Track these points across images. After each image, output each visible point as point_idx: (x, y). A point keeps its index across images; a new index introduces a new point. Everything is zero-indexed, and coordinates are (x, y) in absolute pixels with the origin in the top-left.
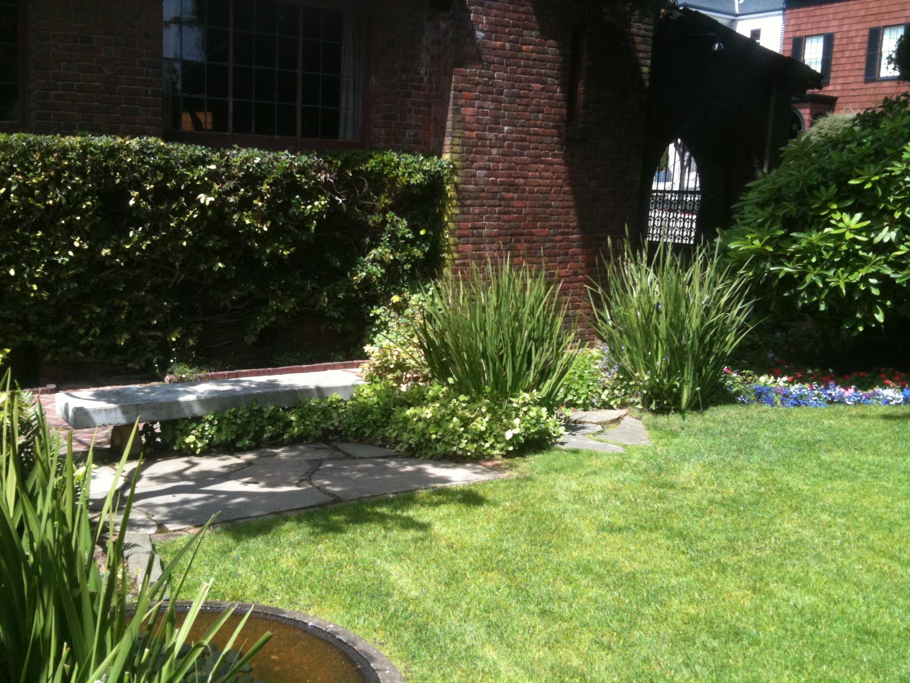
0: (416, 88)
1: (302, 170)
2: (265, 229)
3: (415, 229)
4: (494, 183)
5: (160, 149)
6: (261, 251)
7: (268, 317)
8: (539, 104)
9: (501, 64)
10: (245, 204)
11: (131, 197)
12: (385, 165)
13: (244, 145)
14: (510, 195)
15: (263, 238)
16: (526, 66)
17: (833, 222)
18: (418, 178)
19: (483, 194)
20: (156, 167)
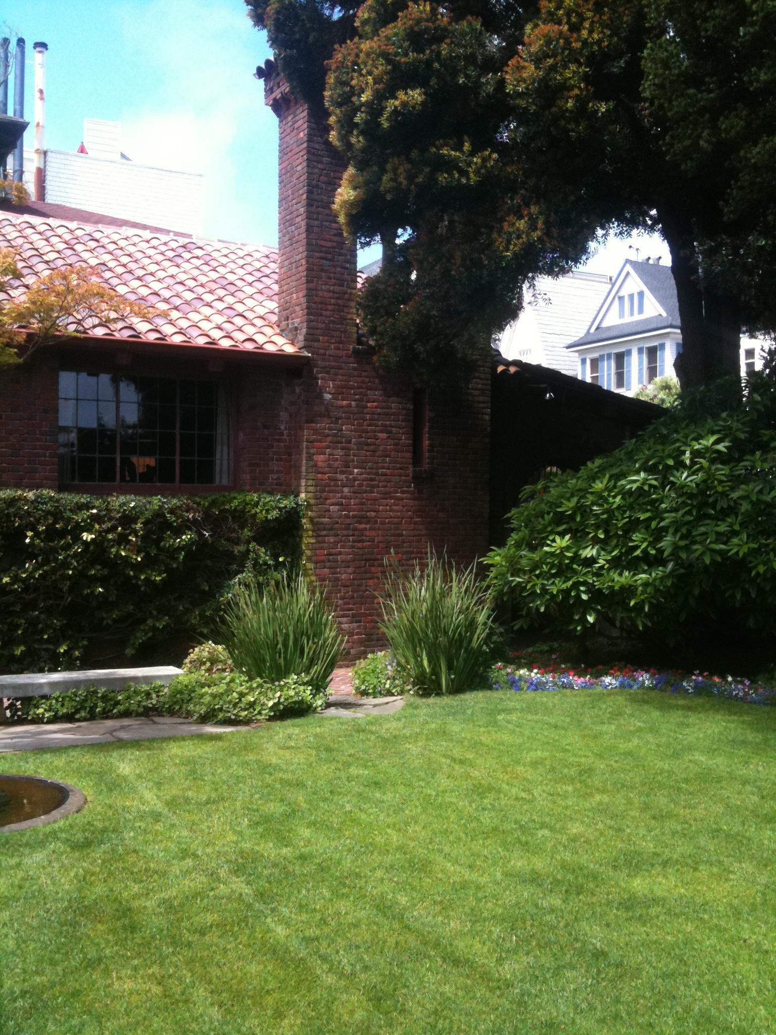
0: (277, 441)
1: (172, 511)
2: (139, 559)
3: (275, 557)
4: (347, 516)
5: (51, 498)
6: (136, 577)
7: (146, 634)
8: (385, 450)
9: (349, 418)
10: (122, 540)
11: (27, 537)
12: (247, 504)
13: (123, 491)
14: (363, 526)
15: (138, 567)
16: (371, 419)
17: (548, 542)
18: (274, 514)
19: (336, 526)
20: (48, 513)
